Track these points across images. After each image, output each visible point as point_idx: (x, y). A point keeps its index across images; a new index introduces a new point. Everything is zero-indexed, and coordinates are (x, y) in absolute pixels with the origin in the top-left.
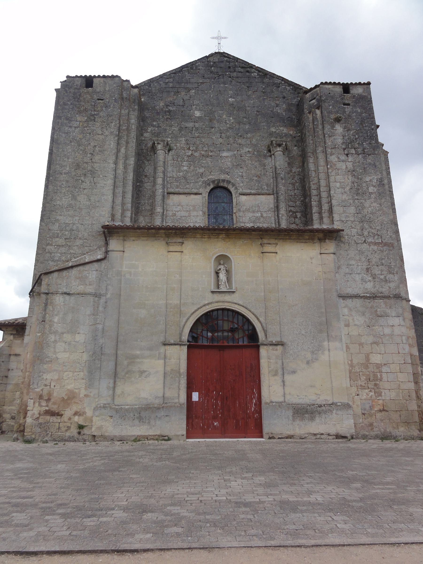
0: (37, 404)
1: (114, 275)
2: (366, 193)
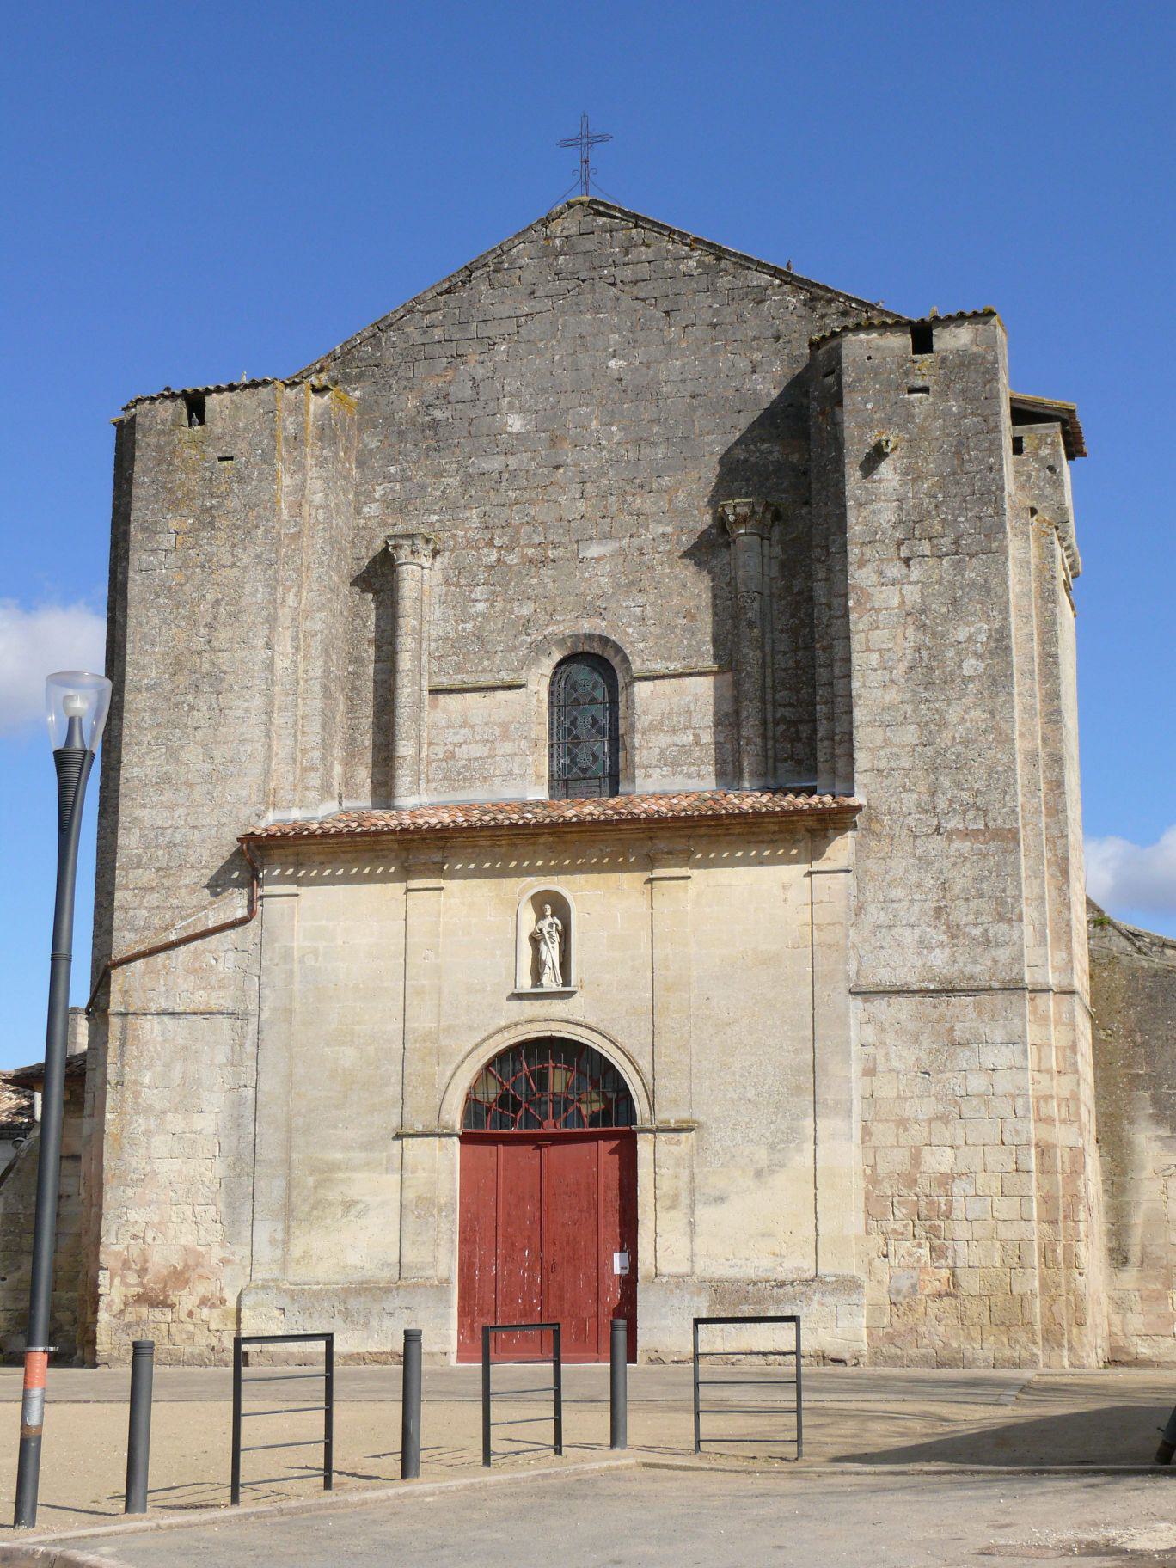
0: (117, 1281)
1: (276, 961)
2: (953, 681)
